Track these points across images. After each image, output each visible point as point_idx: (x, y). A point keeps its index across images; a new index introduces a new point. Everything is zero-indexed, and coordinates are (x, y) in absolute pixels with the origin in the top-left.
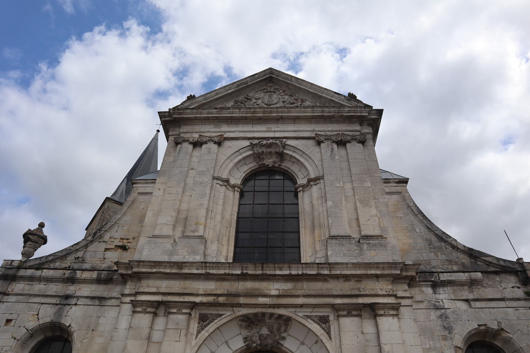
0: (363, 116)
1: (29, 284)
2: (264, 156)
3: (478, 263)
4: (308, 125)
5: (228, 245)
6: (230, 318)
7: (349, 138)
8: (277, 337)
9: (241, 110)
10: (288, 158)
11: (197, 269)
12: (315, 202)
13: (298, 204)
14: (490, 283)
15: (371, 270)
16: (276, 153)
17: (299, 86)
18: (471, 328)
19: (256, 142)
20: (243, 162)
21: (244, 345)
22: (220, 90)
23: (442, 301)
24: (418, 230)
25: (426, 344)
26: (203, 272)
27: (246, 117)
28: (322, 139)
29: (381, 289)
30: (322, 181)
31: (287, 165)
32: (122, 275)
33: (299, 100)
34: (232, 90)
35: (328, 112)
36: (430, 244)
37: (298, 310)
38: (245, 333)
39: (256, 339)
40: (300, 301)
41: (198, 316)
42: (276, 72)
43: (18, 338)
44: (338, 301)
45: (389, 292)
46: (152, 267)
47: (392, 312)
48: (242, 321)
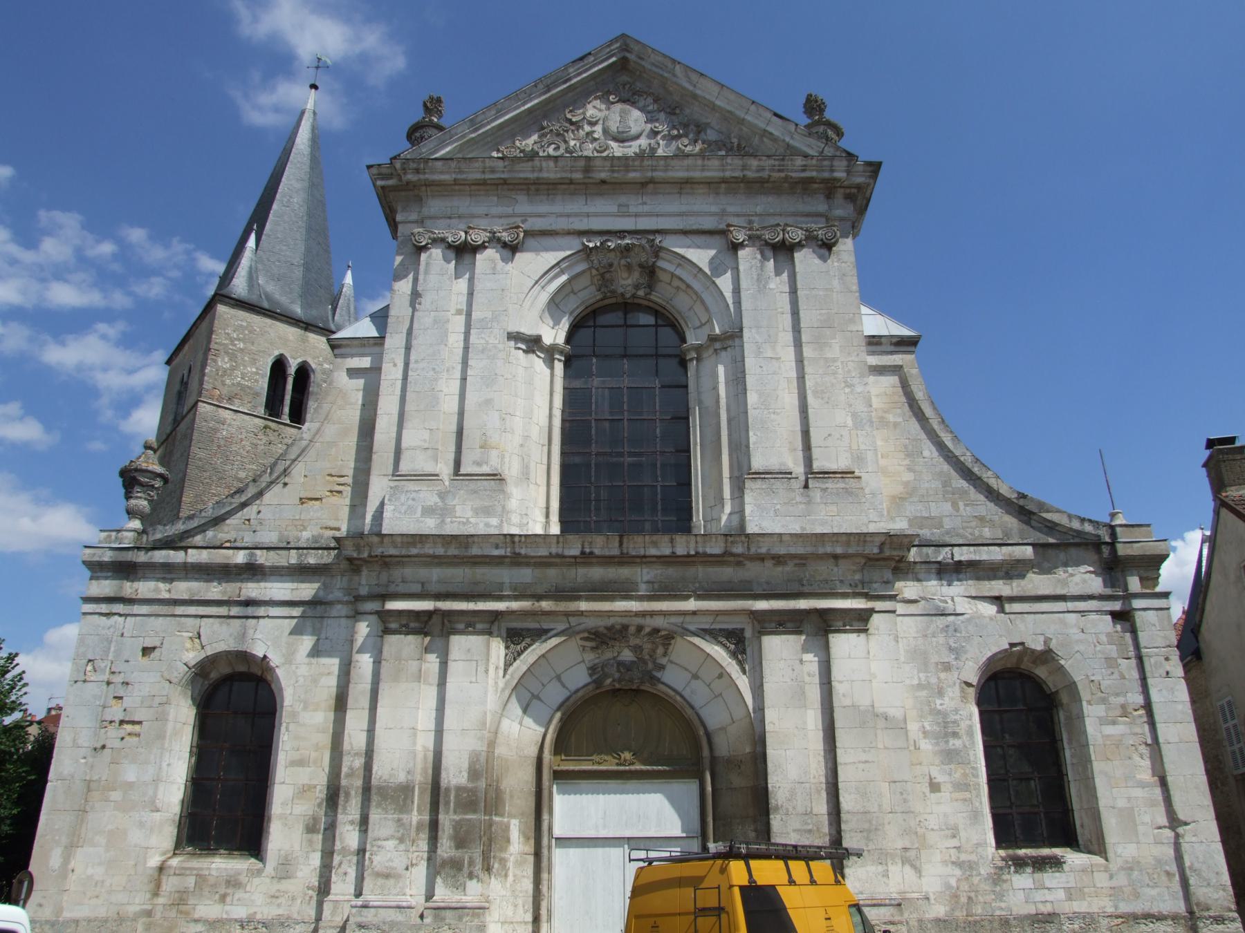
0: (835, 179)
13: (686, 387)
18: (995, 650)
21: (588, 680)
23: (953, 600)
29: (841, 581)
33: (692, 127)
36: (946, 484)
38: (590, 657)
44: (762, 605)
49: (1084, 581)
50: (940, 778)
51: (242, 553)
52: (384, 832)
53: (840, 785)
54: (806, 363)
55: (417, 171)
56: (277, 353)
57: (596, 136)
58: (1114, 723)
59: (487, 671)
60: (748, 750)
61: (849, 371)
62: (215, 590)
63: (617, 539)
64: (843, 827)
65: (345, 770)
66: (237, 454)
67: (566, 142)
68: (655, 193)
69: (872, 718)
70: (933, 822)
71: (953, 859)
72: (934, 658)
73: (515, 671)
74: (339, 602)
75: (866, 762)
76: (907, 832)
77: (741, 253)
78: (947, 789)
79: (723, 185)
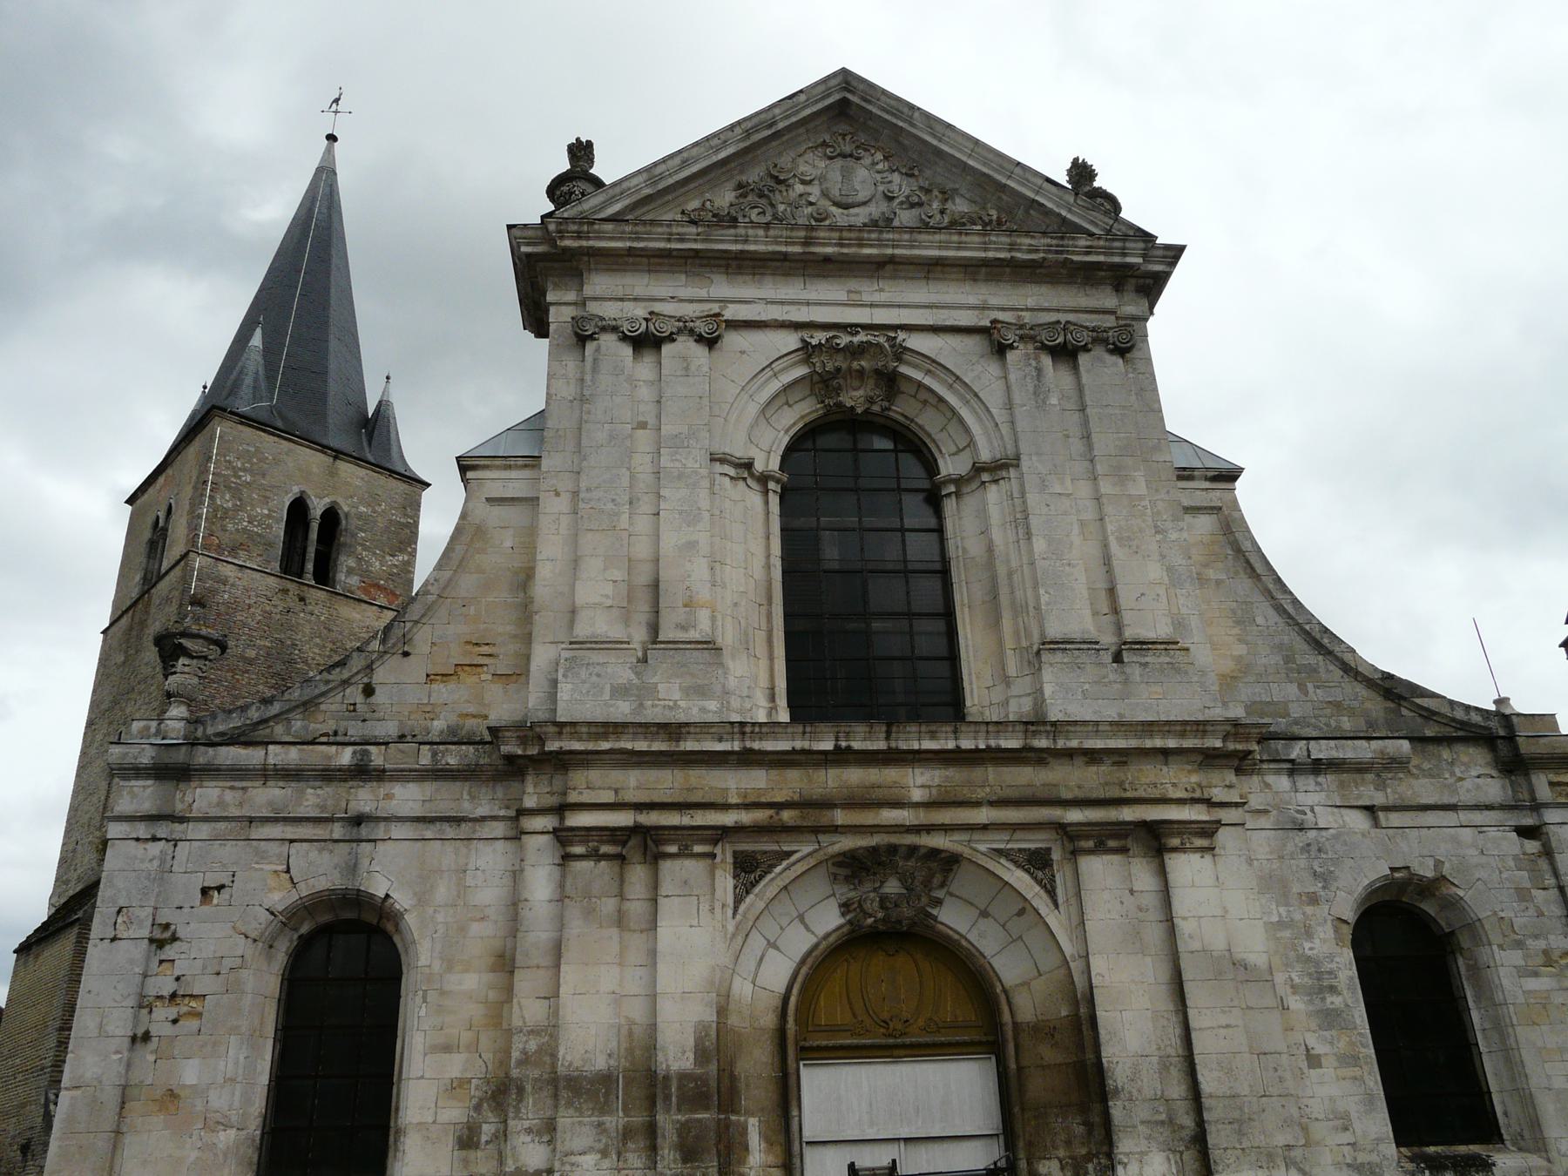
1: (232, 788)
2: (841, 381)
3: (1405, 712)
4: (967, 287)
5: (771, 658)
6: (812, 862)
7: (1085, 337)
8: (924, 900)
9: (771, 233)
10: (904, 386)
11: (720, 740)
12: (997, 536)
14: (1426, 766)
15: (1151, 737)
16: (877, 372)
17: (935, 142)
19: (819, 337)
20: (782, 399)
22: (695, 151)
23: (1312, 810)
24: (1260, 620)
25: (1270, 913)
26: (737, 746)
27: (785, 254)
28: (1011, 337)
29: (1174, 785)
30: (1013, 473)
31: (903, 408)
32: (510, 759)
33: (936, 192)
34: (730, 150)
35: (1029, 247)
36: (1288, 659)
37: (977, 836)
38: (845, 892)
39: (872, 905)
40: (983, 815)
41: (730, 859)
42: (861, 87)
43: (253, 935)
44: (1074, 816)
45: (1194, 791)
46: (597, 737)
47: (1199, 842)
48: (839, 864)
49: (1478, 787)
50: (1319, 1049)
51: (349, 750)
52: (578, 1143)
53: (1197, 1059)
54: (1104, 500)
55: (579, 236)
56: (296, 489)
57: (812, 199)
58: (1536, 974)
59: (712, 910)
60: (1064, 1013)
61: (1158, 513)
62: (312, 799)
63: (884, 728)
64: (1206, 1116)
65: (515, 1055)
66: (244, 625)
67: (773, 206)
68: (894, 277)
69: (1236, 969)
70: (1317, 1109)
71: (1349, 1161)
72: (1296, 888)
73: (748, 909)
74: (494, 818)
75: (1228, 1026)
76: (1287, 1122)
77: (1011, 356)
78: (1329, 1063)
79: (983, 270)
